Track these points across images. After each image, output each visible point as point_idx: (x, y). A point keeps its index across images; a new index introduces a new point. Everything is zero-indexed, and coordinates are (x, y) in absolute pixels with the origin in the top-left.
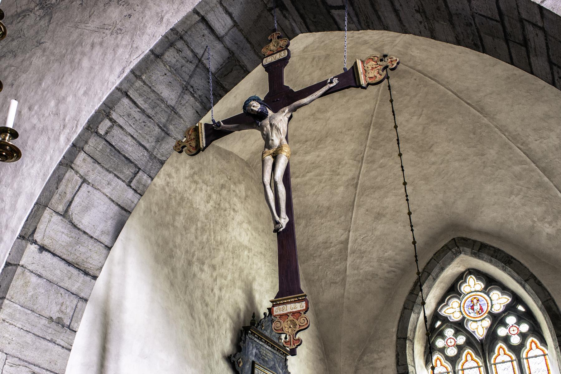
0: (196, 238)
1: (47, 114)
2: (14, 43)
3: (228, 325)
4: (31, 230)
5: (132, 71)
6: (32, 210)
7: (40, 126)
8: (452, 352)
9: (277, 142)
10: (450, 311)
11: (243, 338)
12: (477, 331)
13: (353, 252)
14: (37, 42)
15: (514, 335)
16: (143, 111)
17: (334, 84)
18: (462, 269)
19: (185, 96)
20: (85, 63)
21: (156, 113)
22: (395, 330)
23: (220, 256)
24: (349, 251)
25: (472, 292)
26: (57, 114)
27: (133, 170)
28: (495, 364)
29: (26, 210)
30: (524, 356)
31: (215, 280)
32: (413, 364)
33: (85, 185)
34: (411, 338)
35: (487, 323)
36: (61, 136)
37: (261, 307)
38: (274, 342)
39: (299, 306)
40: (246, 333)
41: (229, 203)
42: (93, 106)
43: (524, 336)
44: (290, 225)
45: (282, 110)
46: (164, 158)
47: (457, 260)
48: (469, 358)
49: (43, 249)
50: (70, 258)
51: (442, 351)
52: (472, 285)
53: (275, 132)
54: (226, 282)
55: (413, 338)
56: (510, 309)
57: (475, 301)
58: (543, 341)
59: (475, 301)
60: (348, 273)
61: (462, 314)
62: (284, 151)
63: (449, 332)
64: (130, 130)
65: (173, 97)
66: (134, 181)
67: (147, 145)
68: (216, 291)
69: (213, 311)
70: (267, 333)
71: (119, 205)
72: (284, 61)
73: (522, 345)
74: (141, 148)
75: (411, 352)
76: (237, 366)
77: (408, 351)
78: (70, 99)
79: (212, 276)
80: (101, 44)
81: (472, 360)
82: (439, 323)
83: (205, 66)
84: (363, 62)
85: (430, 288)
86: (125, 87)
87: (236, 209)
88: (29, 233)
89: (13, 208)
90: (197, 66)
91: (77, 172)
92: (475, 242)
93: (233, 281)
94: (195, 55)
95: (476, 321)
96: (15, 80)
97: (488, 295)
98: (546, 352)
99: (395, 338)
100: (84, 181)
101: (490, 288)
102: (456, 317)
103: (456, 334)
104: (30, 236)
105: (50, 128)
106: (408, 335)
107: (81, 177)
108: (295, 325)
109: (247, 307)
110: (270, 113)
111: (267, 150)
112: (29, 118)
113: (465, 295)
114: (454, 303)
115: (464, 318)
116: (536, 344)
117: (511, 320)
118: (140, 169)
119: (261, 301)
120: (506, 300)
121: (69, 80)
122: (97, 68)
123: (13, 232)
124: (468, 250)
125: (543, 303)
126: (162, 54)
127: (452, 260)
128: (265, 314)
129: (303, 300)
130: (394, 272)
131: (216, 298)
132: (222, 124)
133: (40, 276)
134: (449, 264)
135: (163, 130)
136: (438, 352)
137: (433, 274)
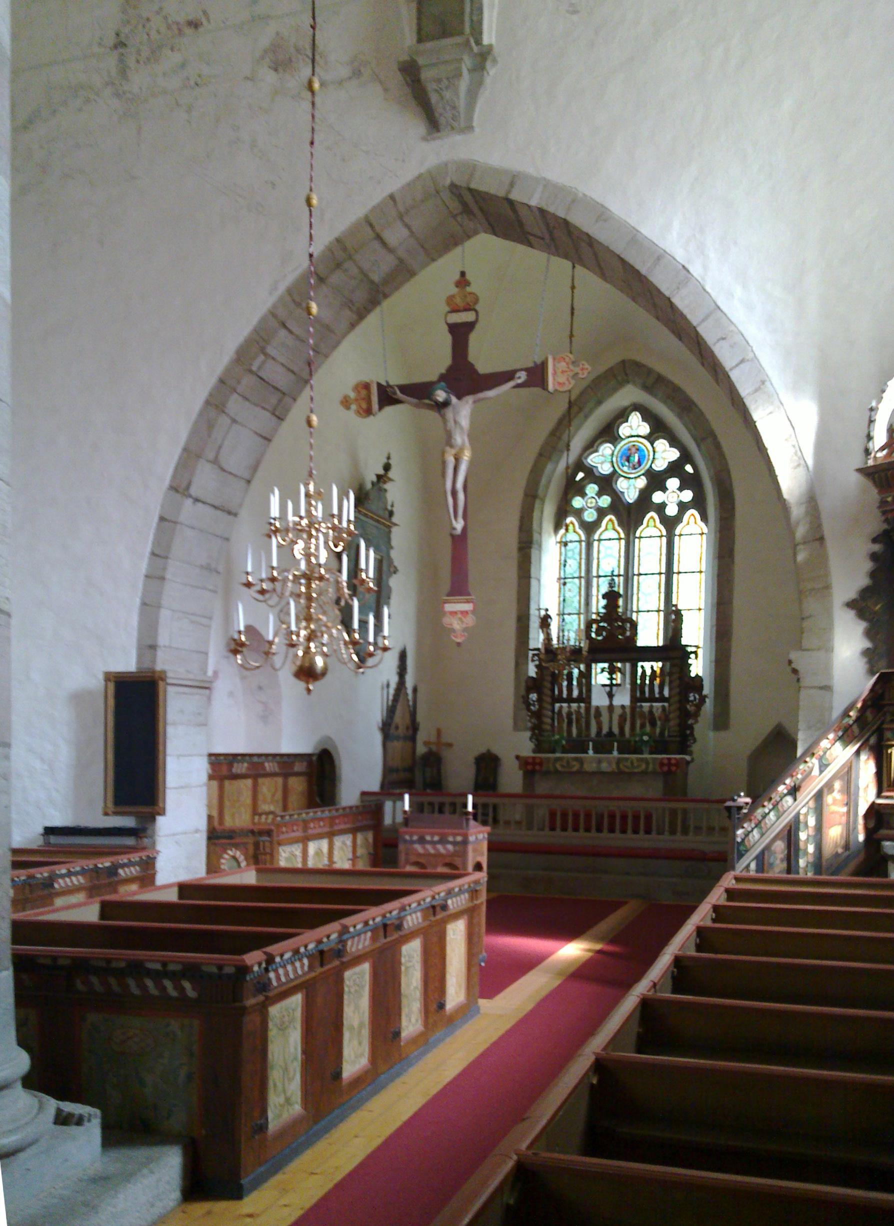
8: (590, 516)
12: (628, 492)
35: (642, 482)
39: (468, 607)
44: (465, 529)
48: (610, 526)
49: (197, 500)
50: (216, 504)
51: (578, 513)
52: (634, 427)
56: (674, 469)
57: (633, 450)
58: (704, 518)
59: (633, 450)
62: (465, 455)
63: (592, 489)
67: (295, 369)
71: (261, 436)
72: (470, 326)
73: (678, 519)
77: (536, 514)
82: (580, 475)
85: (579, 427)
86: (281, 313)
91: (228, 415)
94: (362, 271)
97: (652, 444)
100: (234, 421)
101: (656, 435)
102: (605, 469)
103: (600, 494)
110: (454, 400)
114: (606, 449)
117: (673, 483)
118: (284, 394)
120: (674, 454)
132: (398, 392)
133: (193, 528)
137: (586, 410)
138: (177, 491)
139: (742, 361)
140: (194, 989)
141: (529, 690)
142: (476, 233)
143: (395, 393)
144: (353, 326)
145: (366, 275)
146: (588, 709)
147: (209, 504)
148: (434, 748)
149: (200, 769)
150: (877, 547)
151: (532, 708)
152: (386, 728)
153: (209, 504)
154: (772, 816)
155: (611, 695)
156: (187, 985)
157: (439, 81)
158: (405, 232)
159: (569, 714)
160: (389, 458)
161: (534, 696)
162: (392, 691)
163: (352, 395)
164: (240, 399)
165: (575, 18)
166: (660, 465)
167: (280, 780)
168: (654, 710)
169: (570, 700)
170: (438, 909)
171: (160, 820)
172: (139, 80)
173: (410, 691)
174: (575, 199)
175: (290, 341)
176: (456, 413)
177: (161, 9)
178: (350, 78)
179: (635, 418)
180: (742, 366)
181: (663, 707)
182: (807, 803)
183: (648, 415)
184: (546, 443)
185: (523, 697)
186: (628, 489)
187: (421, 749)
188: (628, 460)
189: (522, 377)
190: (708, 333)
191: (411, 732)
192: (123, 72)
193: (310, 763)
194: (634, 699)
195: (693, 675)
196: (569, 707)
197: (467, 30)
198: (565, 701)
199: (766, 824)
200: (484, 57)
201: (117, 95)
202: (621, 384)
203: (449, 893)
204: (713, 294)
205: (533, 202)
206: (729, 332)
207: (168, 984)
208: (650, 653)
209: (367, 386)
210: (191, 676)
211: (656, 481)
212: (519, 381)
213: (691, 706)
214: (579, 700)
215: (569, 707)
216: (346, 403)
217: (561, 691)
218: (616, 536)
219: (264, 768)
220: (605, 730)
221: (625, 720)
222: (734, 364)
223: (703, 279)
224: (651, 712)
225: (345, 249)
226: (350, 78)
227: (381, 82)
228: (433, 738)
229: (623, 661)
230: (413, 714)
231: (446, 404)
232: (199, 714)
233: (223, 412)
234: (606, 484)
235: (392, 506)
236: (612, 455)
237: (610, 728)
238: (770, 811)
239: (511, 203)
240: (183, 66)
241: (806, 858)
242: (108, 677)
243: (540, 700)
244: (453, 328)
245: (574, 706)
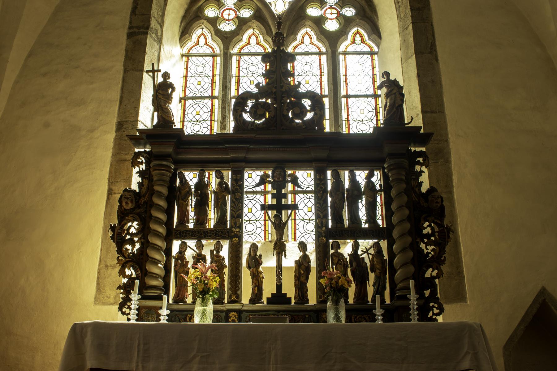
15: (331, 19)
32: (160, 20)
73: (341, 34)
81: (258, 43)
116: (361, 37)
136: (205, 22)
147: (399, 283)
151: (128, 247)
153: (399, 283)
161: (134, 227)
185: (113, 228)
198: (191, 235)
213: (427, 244)
217: (184, 218)
220: (269, 290)
221: (308, 270)
237: (279, 287)
243: (144, 231)
245: (208, 246)
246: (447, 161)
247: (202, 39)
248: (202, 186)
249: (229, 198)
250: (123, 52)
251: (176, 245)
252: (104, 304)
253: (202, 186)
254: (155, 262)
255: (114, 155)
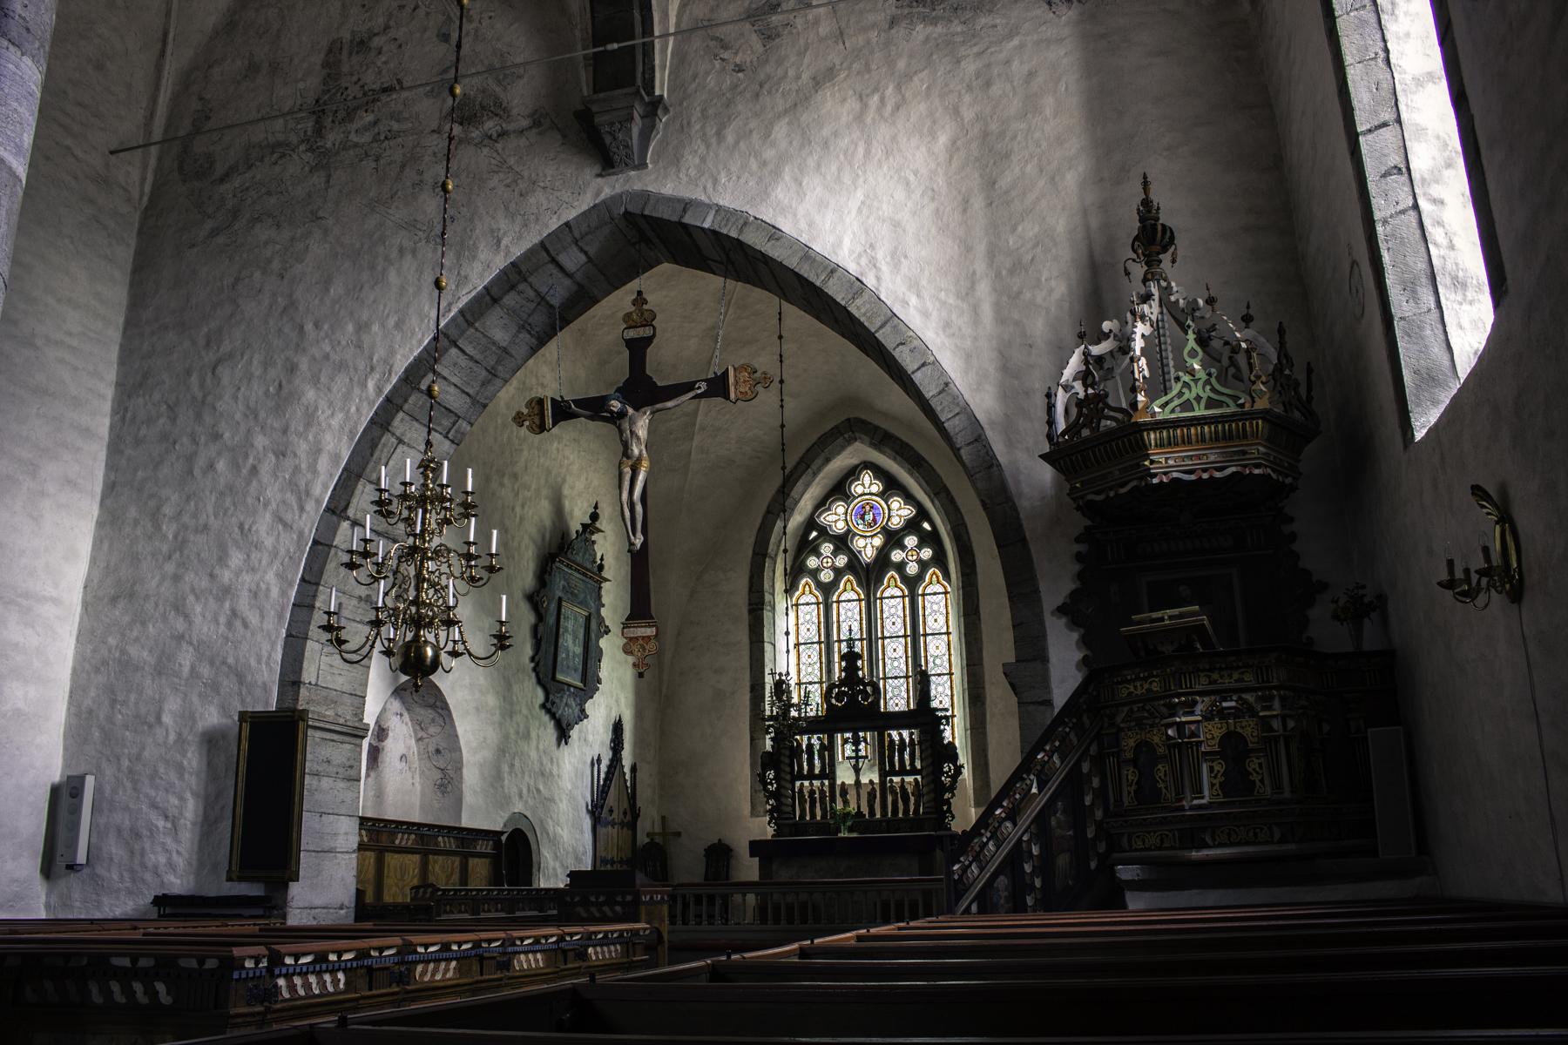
0: (496, 440)
1: (344, 343)
2: (273, 200)
3: (530, 553)
4: (343, 504)
5: (461, 312)
6: (340, 477)
7: (335, 357)
8: (826, 576)
9: (636, 452)
10: (832, 518)
11: (549, 569)
13: (703, 429)
14: (312, 212)
16: (471, 358)
17: (703, 390)
18: (855, 461)
19: (521, 336)
20: (393, 277)
21: (486, 357)
22: (752, 540)
23: (523, 460)
24: (697, 427)
25: (865, 494)
26: (359, 346)
27: (454, 418)
28: (881, 599)
29: (331, 475)
30: (920, 592)
31: (517, 494)
33: (400, 446)
34: (773, 554)
35: (878, 541)
36: (369, 380)
37: (572, 518)
38: (587, 570)
39: (651, 631)
40: (554, 561)
41: (537, 376)
42: (411, 351)
43: (924, 565)
44: (644, 544)
45: (643, 410)
46: (487, 401)
47: (850, 449)
51: (814, 573)
53: (634, 441)
54: (529, 494)
55: (776, 555)
56: (912, 526)
57: (868, 508)
58: (947, 576)
59: (868, 508)
60: (693, 457)
61: (848, 525)
63: (827, 548)
64: (454, 380)
65: (506, 338)
66: (453, 431)
67: (471, 391)
68: (518, 509)
69: (513, 538)
70: (579, 559)
72: (648, 341)
73: (920, 577)
74: (464, 395)
75: (771, 574)
76: (540, 608)
78: (375, 328)
79: (513, 490)
80: (414, 252)
82: (814, 534)
83: (548, 303)
84: (735, 369)
85: (807, 486)
87: (545, 383)
88: (341, 508)
89: (313, 469)
90: (539, 304)
91: (393, 434)
92: (877, 428)
93: (538, 491)
94: (538, 293)
95: (865, 537)
96: (286, 270)
97: (886, 503)
98: (949, 589)
99: (750, 553)
100: (400, 441)
102: (840, 527)
103: (835, 553)
104: (342, 511)
105: (351, 364)
106: (769, 551)
107: (397, 438)
108: (644, 649)
109: (554, 523)
110: (631, 411)
111: (625, 459)
112: (318, 342)
113: (856, 498)
114: (840, 508)
115: (849, 531)
116: (937, 577)
118: (459, 417)
119: (572, 511)
121: (372, 298)
122: (411, 290)
123: (318, 502)
124: (867, 439)
125: (952, 529)
126: (501, 298)
127: (843, 448)
128: (577, 532)
129: (653, 626)
130: (759, 458)
131: (518, 519)
134: (839, 453)
135: (491, 373)
137: (814, 467)
138: (333, 512)
139: (924, 365)
140: (168, 993)
141: (765, 768)
142: (659, 263)
143: (570, 407)
144: (534, 351)
145: (543, 298)
146: (832, 786)
148: (658, 840)
149: (347, 835)
150: (1082, 548)
152: (596, 811)
154: (991, 846)
155: (857, 770)
156: (161, 987)
157: (612, 124)
158: (583, 258)
159: (812, 792)
160: (596, 507)
161: (771, 774)
162: (604, 768)
163: (525, 411)
164: (407, 418)
165: (740, 75)
166: (896, 523)
167: (457, 860)
168: (907, 786)
169: (811, 776)
170: (571, 955)
171: (295, 889)
172: (332, 138)
173: (627, 770)
174: (745, 221)
175: (463, 361)
176: (632, 422)
177: (359, 80)
178: (530, 128)
179: (867, 477)
180: (923, 369)
181: (916, 780)
182: (1029, 827)
183: (880, 473)
184: (774, 500)
185: (759, 775)
186: (865, 547)
187: (642, 839)
188: (863, 518)
189: (703, 386)
190: (886, 337)
191: (629, 817)
192: (319, 130)
193: (497, 844)
194: (883, 774)
195: (946, 742)
196: (811, 784)
197: (639, 81)
198: (805, 778)
199: (985, 856)
200: (655, 106)
201: (311, 150)
202: (850, 442)
203: (589, 938)
204: (888, 303)
205: (706, 225)
206: (907, 337)
207: (138, 987)
208: (899, 720)
209: (540, 402)
210: (341, 721)
211: (893, 539)
212: (699, 392)
214: (822, 776)
215: (811, 784)
216: (519, 419)
218: (855, 597)
219: (437, 844)
222: (916, 368)
223: (877, 289)
224: (902, 787)
225: (520, 272)
226: (530, 128)
227: (559, 129)
228: (658, 829)
229: (865, 730)
230: (632, 797)
231: (622, 414)
232: (351, 767)
233: (388, 431)
234: (842, 542)
235: (602, 559)
236: (846, 513)
238: (989, 840)
239: (685, 227)
240: (375, 123)
241: (1033, 895)
242: (243, 716)
244: (630, 343)
245: (817, 783)
246: (984, 704)
247: (807, 588)
248: (810, 746)
249: (826, 753)
250: (747, 628)
251: (798, 784)
252: (758, 816)
253: (810, 746)
254: (786, 797)
255: (751, 710)
